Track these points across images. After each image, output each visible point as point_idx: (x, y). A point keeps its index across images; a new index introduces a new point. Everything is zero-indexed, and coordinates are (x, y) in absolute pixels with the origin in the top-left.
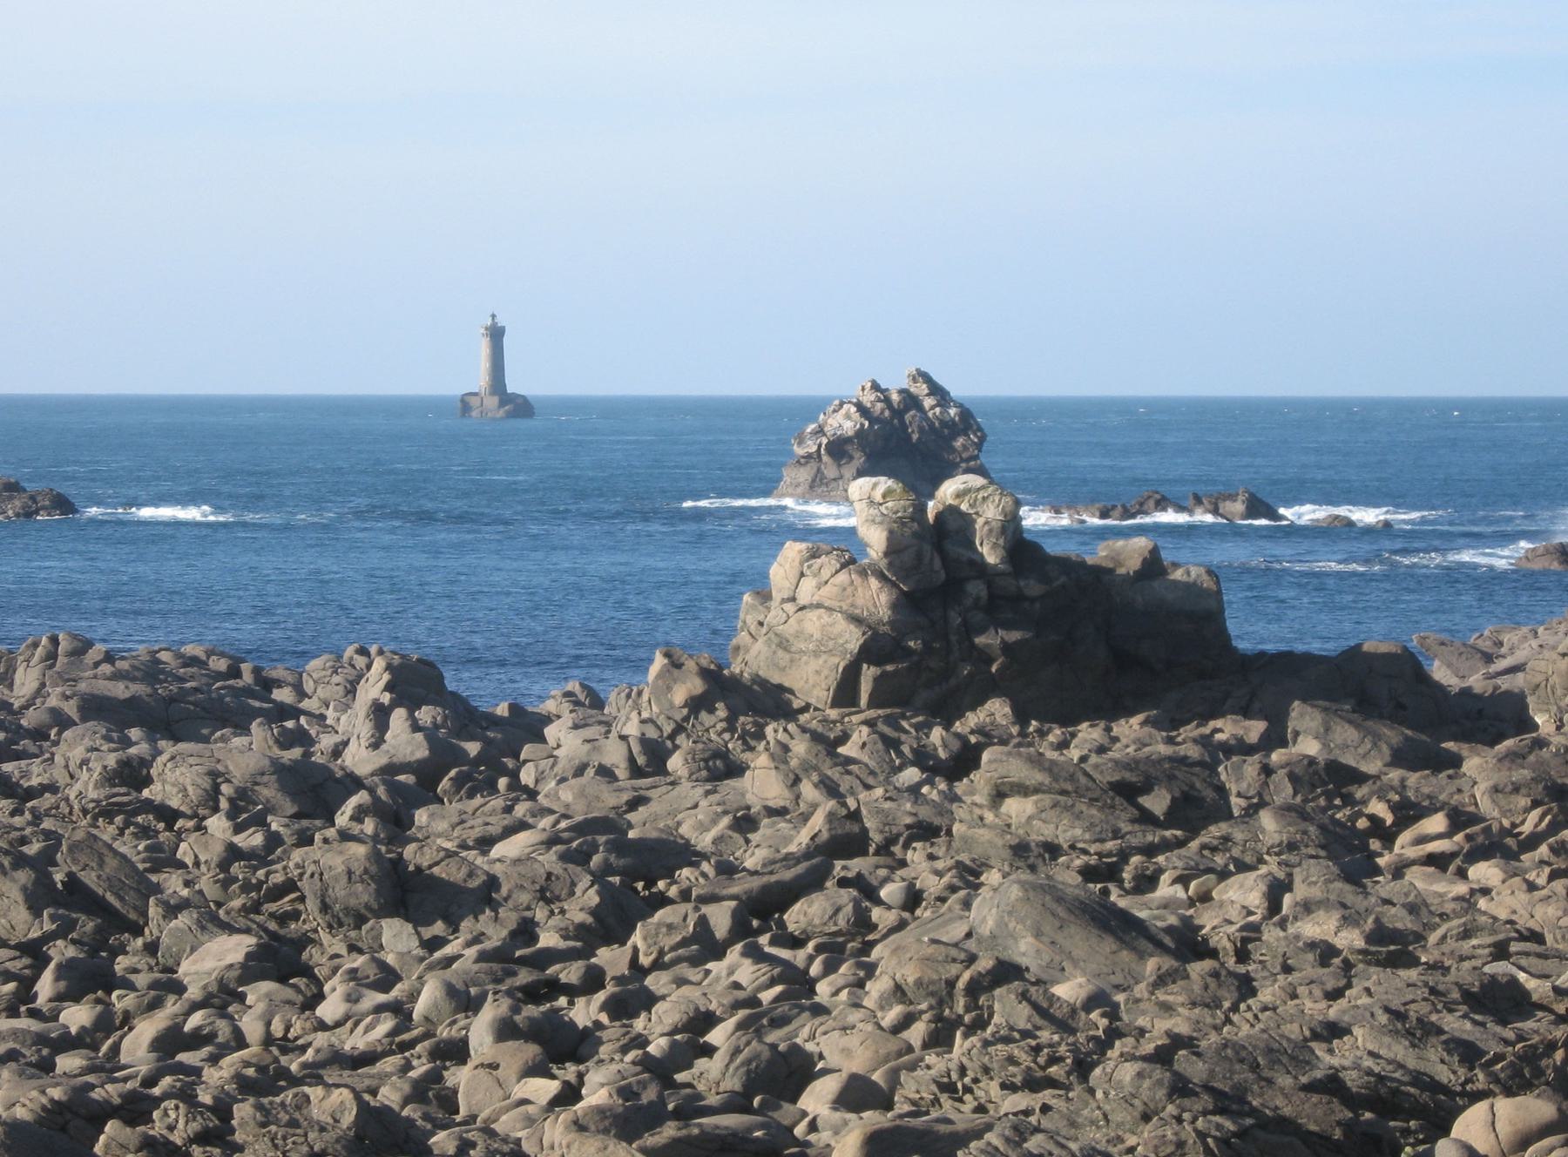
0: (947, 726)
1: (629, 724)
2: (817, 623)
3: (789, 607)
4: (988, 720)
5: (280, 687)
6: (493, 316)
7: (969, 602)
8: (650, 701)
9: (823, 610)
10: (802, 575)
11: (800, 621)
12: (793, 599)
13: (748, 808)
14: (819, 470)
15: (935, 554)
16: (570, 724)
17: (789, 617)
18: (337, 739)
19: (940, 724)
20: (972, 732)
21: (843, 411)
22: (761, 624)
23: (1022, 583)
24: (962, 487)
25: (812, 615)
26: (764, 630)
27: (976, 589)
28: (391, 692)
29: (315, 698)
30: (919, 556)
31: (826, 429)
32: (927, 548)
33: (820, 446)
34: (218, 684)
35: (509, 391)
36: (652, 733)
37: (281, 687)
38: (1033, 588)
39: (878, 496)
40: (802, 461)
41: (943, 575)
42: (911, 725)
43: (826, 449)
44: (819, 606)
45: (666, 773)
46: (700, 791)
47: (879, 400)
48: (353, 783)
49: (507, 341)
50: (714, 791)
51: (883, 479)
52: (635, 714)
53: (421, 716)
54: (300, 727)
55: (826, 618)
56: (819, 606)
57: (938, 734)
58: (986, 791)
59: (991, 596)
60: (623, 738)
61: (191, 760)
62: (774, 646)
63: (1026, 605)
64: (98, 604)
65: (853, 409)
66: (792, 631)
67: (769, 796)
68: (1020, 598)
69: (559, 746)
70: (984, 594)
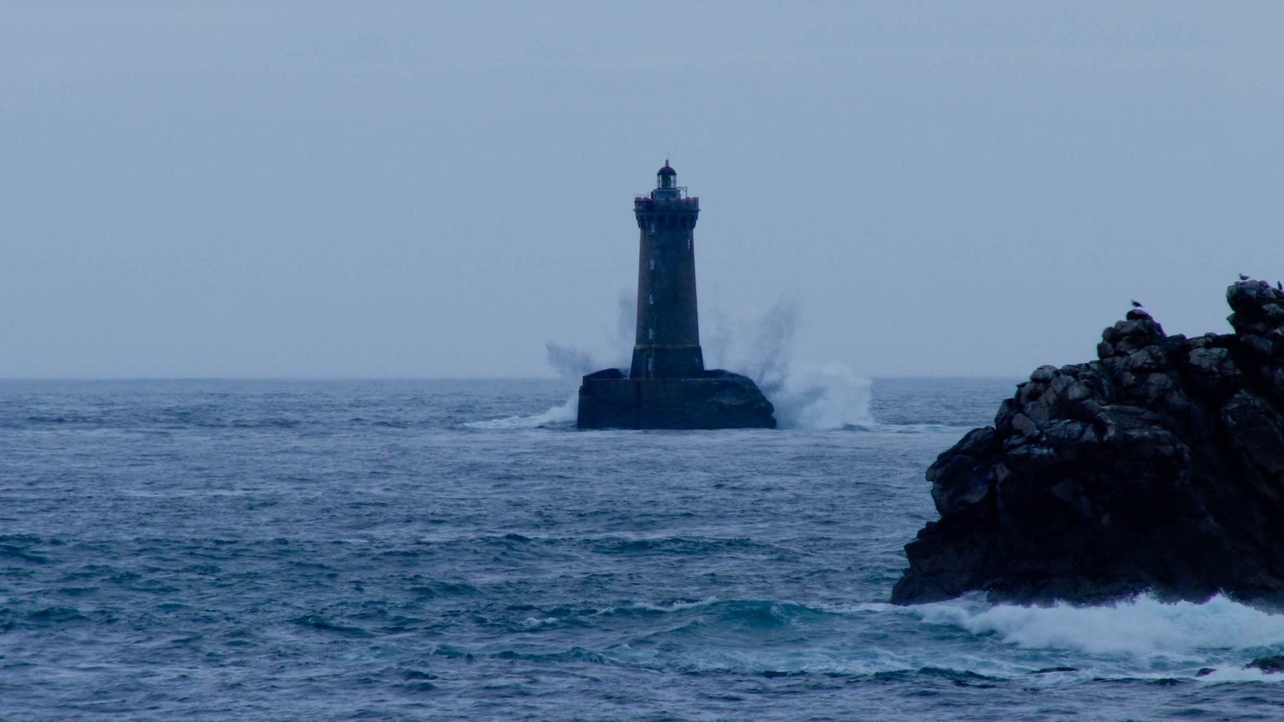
6: (666, 174)
35: (710, 363)
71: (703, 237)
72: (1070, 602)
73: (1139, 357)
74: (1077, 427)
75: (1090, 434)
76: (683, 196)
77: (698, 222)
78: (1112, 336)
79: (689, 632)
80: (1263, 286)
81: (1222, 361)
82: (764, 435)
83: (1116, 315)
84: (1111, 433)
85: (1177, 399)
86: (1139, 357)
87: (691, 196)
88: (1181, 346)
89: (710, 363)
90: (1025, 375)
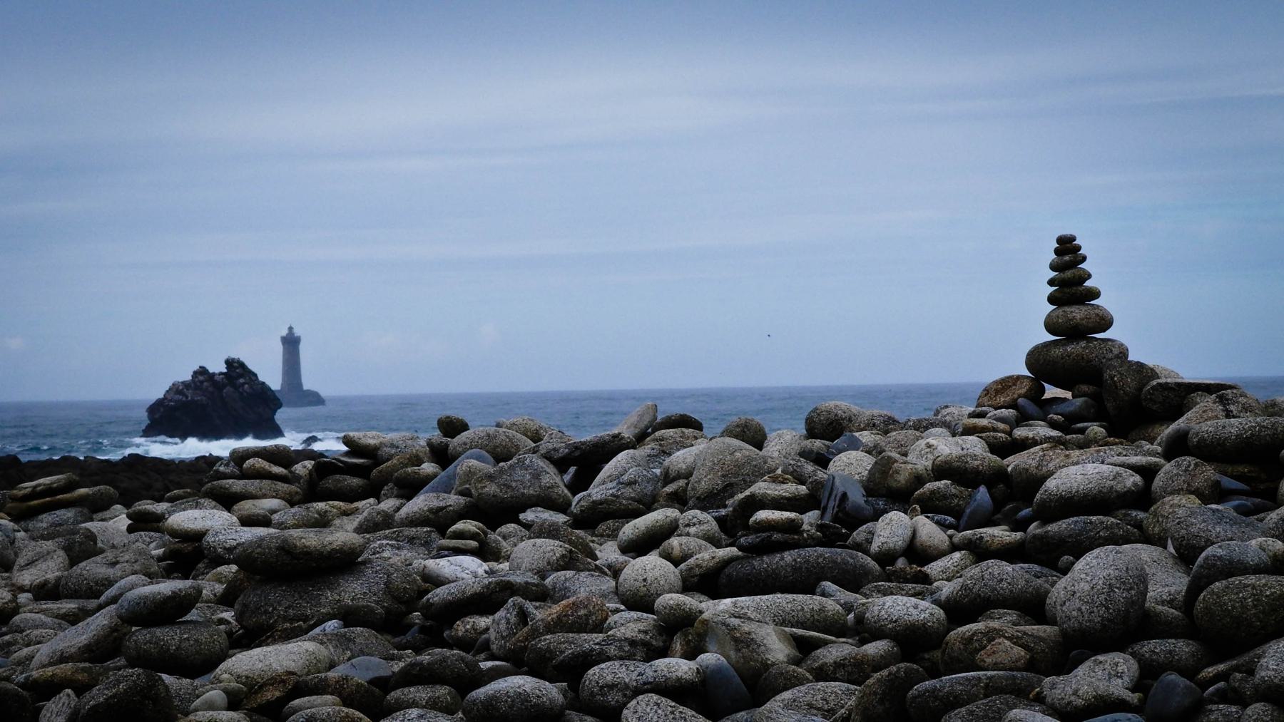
6: (291, 329)
72: (241, 450)
73: (201, 378)
74: (181, 397)
75: (184, 399)
76: (296, 335)
78: (195, 373)
80: (234, 359)
81: (223, 379)
83: (196, 368)
84: (189, 398)
85: (211, 389)
86: (201, 378)
87: (298, 335)
88: (214, 374)
89: (306, 387)
90: (171, 384)
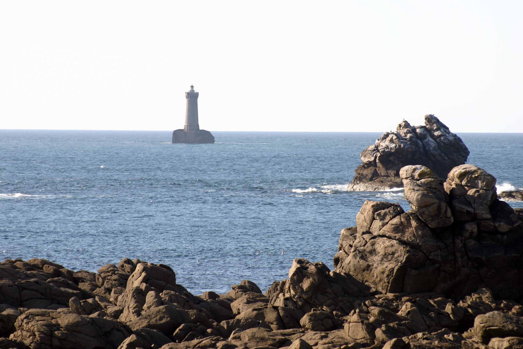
0: (455, 303)
1: (278, 300)
2: (382, 246)
3: (366, 236)
4: (478, 300)
5: (83, 281)
6: (192, 87)
7: (467, 234)
8: (289, 288)
9: (386, 238)
10: (374, 219)
11: (373, 244)
12: (368, 232)
13: (347, 344)
14: (375, 170)
15: (448, 208)
16: (245, 301)
17: (366, 242)
18: (116, 308)
19: (451, 302)
20: (469, 306)
21: (389, 138)
22: (351, 246)
23: (497, 225)
24: (463, 171)
25: (380, 240)
26: (353, 250)
27: (472, 227)
28: (146, 283)
29: (103, 288)
30: (439, 208)
31: (379, 148)
32: (444, 205)
33: (376, 157)
34: (49, 280)
35: (201, 129)
36: (291, 306)
37: (84, 282)
38: (503, 227)
39: (416, 174)
40: (366, 166)
41: (452, 220)
42: (435, 302)
43: (379, 160)
44: (383, 236)
45: (300, 326)
46: (319, 335)
47: (410, 133)
48: (127, 330)
49: (200, 101)
50: (326, 337)
51: (418, 166)
52: (281, 294)
53: (163, 296)
54: (95, 301)
55: (388, 243)
56: (383, 236)
57: (450, 307)
58: (480, 335)
59: (479, 230)
60: (276, 308)
61: (37, 318)
62: (358, 258)
63: (499, 236)
64: (25, 168)
65: (395, 137)
66: (368, 250)
67: (358, 338)
68: (496, 232)
69: (239, 313)
70: (475, 230)
71: (199, 100)
77: (198, 97)
79: (475, 212)
82: (210, 145)
89: (201, 129)
